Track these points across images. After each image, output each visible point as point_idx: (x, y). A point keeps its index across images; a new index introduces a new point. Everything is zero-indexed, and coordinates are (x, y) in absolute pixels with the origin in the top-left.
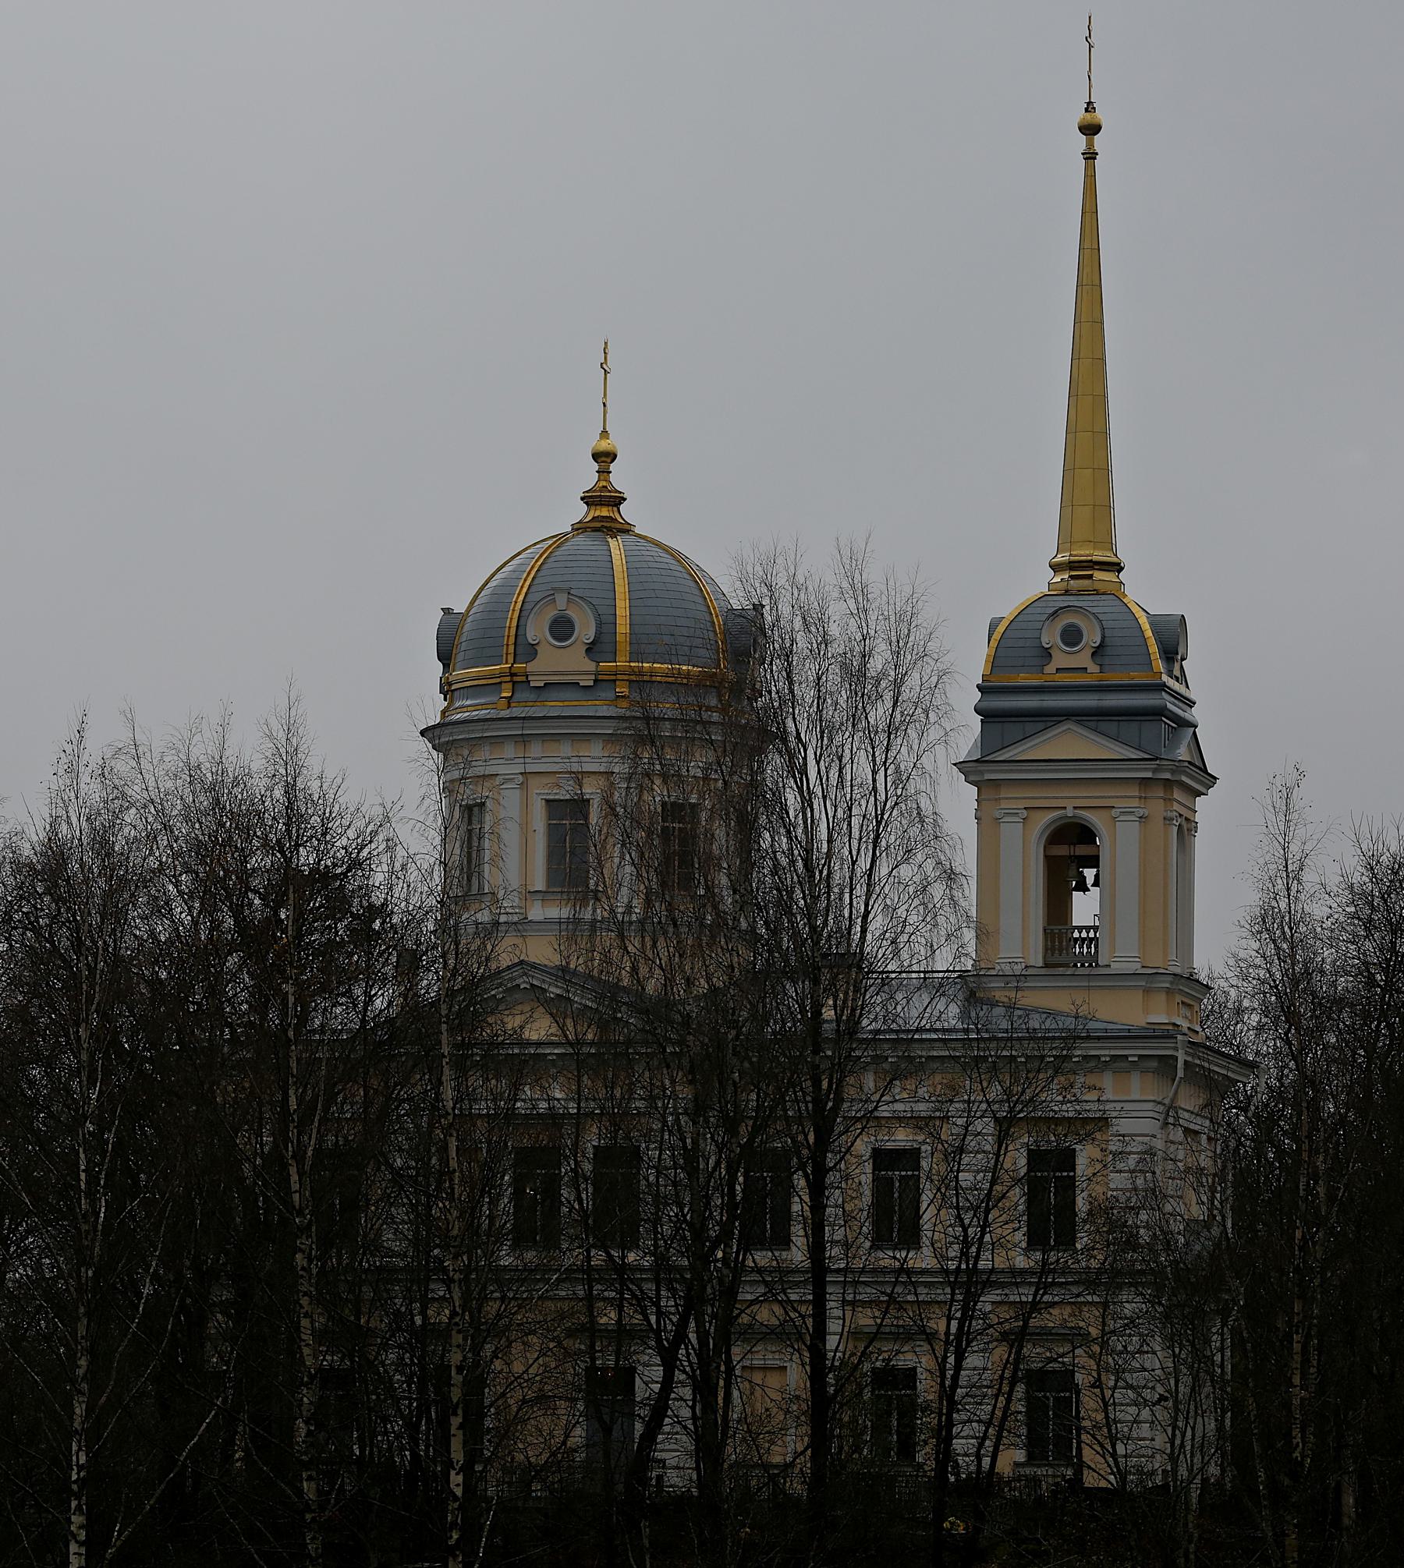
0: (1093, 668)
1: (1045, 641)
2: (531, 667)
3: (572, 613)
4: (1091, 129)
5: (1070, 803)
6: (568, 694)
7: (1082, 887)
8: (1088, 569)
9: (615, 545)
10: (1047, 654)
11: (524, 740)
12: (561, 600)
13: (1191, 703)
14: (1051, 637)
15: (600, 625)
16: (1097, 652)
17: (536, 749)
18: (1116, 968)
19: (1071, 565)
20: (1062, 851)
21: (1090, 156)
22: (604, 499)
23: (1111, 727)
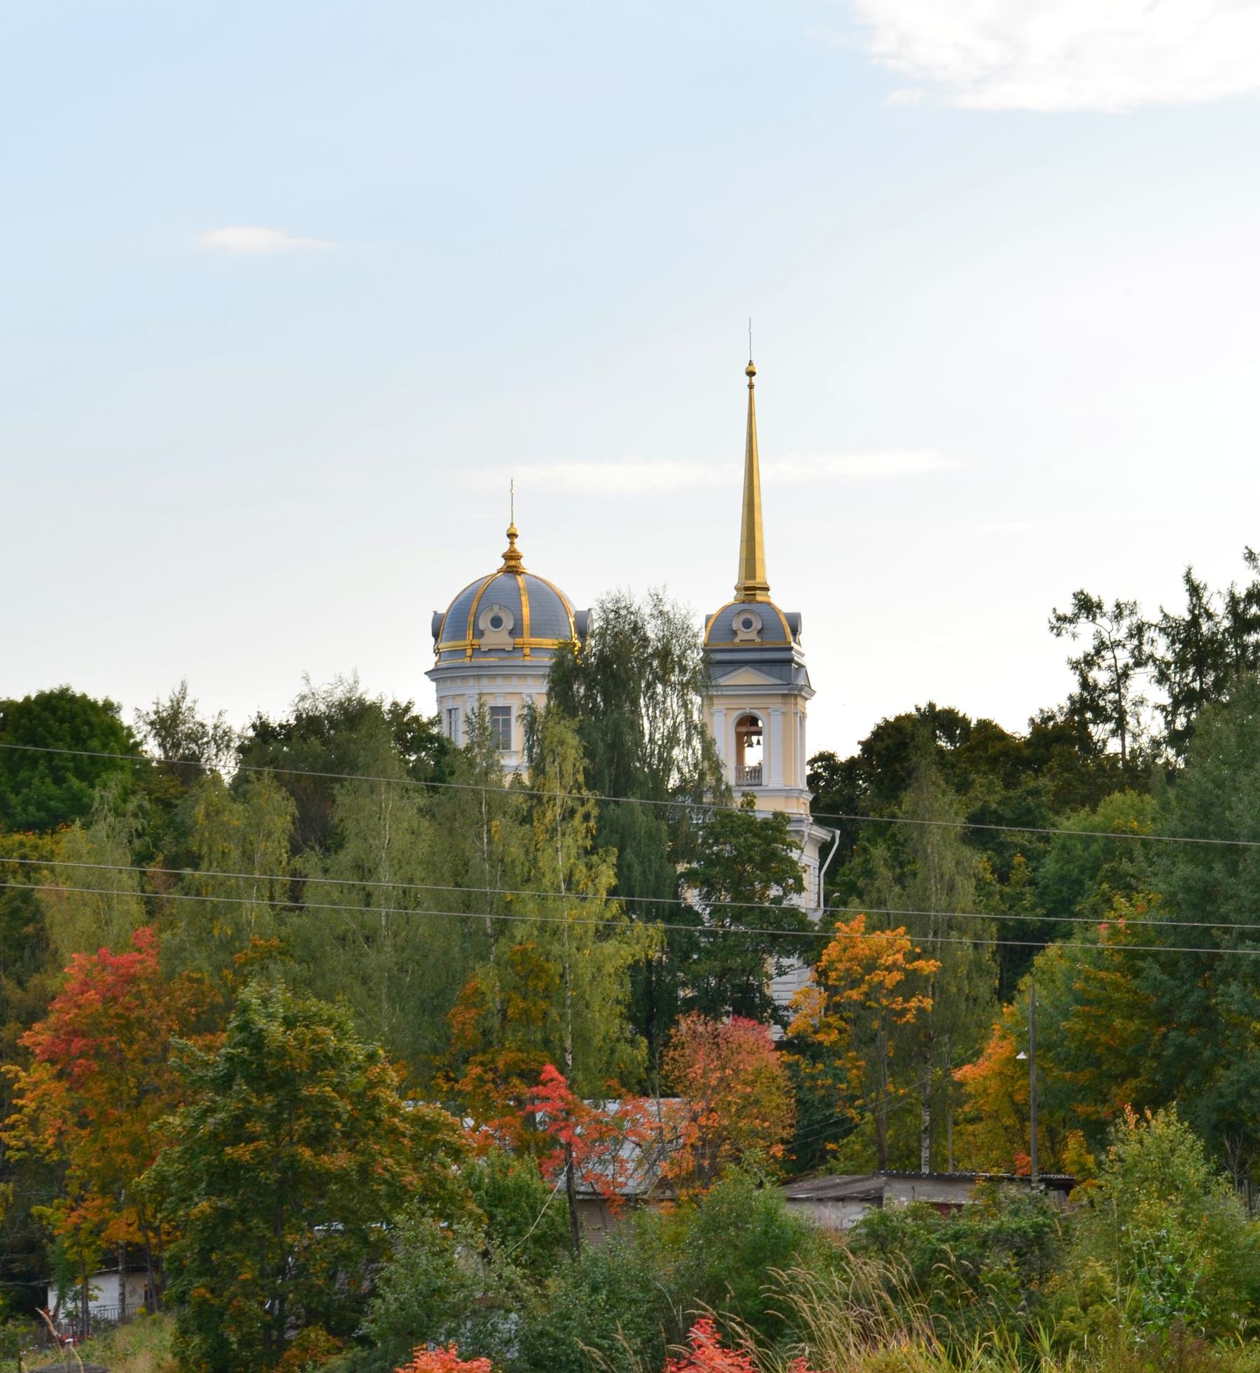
0: (758, 640)
1: (735, 626)
2: (482, 641)
3: (502, 615)
4: (751, 374)
5: (748, 706)
6: (502, 655)
7: (751, 745)
8: (751, 590)
9: (519, 578)
10: (735, 633)
11: (478, 677)
12: (496, 608)
13: (803, 655)
14: (737, 624)
15: (515, 620)
16: (760, 632)
17: (484, 682)
18: (771, 786)
19: (747, 589)
20: (744, 729)
21: (751, 386)
22: (512, 556)
23: (766, 668)
